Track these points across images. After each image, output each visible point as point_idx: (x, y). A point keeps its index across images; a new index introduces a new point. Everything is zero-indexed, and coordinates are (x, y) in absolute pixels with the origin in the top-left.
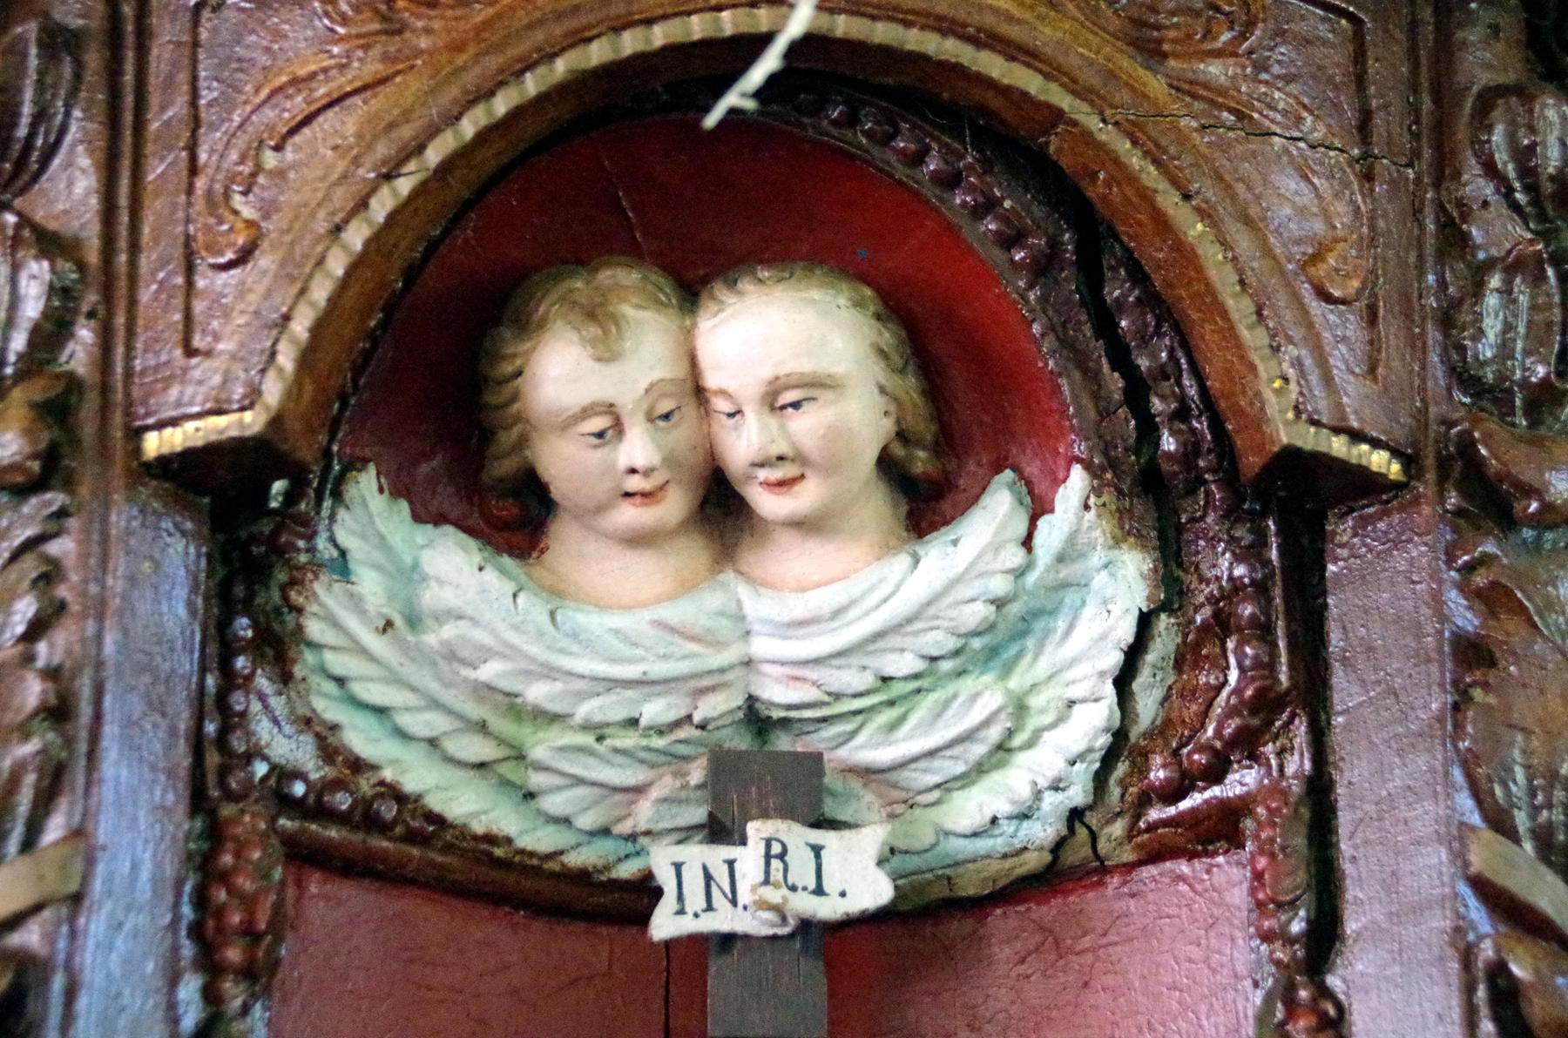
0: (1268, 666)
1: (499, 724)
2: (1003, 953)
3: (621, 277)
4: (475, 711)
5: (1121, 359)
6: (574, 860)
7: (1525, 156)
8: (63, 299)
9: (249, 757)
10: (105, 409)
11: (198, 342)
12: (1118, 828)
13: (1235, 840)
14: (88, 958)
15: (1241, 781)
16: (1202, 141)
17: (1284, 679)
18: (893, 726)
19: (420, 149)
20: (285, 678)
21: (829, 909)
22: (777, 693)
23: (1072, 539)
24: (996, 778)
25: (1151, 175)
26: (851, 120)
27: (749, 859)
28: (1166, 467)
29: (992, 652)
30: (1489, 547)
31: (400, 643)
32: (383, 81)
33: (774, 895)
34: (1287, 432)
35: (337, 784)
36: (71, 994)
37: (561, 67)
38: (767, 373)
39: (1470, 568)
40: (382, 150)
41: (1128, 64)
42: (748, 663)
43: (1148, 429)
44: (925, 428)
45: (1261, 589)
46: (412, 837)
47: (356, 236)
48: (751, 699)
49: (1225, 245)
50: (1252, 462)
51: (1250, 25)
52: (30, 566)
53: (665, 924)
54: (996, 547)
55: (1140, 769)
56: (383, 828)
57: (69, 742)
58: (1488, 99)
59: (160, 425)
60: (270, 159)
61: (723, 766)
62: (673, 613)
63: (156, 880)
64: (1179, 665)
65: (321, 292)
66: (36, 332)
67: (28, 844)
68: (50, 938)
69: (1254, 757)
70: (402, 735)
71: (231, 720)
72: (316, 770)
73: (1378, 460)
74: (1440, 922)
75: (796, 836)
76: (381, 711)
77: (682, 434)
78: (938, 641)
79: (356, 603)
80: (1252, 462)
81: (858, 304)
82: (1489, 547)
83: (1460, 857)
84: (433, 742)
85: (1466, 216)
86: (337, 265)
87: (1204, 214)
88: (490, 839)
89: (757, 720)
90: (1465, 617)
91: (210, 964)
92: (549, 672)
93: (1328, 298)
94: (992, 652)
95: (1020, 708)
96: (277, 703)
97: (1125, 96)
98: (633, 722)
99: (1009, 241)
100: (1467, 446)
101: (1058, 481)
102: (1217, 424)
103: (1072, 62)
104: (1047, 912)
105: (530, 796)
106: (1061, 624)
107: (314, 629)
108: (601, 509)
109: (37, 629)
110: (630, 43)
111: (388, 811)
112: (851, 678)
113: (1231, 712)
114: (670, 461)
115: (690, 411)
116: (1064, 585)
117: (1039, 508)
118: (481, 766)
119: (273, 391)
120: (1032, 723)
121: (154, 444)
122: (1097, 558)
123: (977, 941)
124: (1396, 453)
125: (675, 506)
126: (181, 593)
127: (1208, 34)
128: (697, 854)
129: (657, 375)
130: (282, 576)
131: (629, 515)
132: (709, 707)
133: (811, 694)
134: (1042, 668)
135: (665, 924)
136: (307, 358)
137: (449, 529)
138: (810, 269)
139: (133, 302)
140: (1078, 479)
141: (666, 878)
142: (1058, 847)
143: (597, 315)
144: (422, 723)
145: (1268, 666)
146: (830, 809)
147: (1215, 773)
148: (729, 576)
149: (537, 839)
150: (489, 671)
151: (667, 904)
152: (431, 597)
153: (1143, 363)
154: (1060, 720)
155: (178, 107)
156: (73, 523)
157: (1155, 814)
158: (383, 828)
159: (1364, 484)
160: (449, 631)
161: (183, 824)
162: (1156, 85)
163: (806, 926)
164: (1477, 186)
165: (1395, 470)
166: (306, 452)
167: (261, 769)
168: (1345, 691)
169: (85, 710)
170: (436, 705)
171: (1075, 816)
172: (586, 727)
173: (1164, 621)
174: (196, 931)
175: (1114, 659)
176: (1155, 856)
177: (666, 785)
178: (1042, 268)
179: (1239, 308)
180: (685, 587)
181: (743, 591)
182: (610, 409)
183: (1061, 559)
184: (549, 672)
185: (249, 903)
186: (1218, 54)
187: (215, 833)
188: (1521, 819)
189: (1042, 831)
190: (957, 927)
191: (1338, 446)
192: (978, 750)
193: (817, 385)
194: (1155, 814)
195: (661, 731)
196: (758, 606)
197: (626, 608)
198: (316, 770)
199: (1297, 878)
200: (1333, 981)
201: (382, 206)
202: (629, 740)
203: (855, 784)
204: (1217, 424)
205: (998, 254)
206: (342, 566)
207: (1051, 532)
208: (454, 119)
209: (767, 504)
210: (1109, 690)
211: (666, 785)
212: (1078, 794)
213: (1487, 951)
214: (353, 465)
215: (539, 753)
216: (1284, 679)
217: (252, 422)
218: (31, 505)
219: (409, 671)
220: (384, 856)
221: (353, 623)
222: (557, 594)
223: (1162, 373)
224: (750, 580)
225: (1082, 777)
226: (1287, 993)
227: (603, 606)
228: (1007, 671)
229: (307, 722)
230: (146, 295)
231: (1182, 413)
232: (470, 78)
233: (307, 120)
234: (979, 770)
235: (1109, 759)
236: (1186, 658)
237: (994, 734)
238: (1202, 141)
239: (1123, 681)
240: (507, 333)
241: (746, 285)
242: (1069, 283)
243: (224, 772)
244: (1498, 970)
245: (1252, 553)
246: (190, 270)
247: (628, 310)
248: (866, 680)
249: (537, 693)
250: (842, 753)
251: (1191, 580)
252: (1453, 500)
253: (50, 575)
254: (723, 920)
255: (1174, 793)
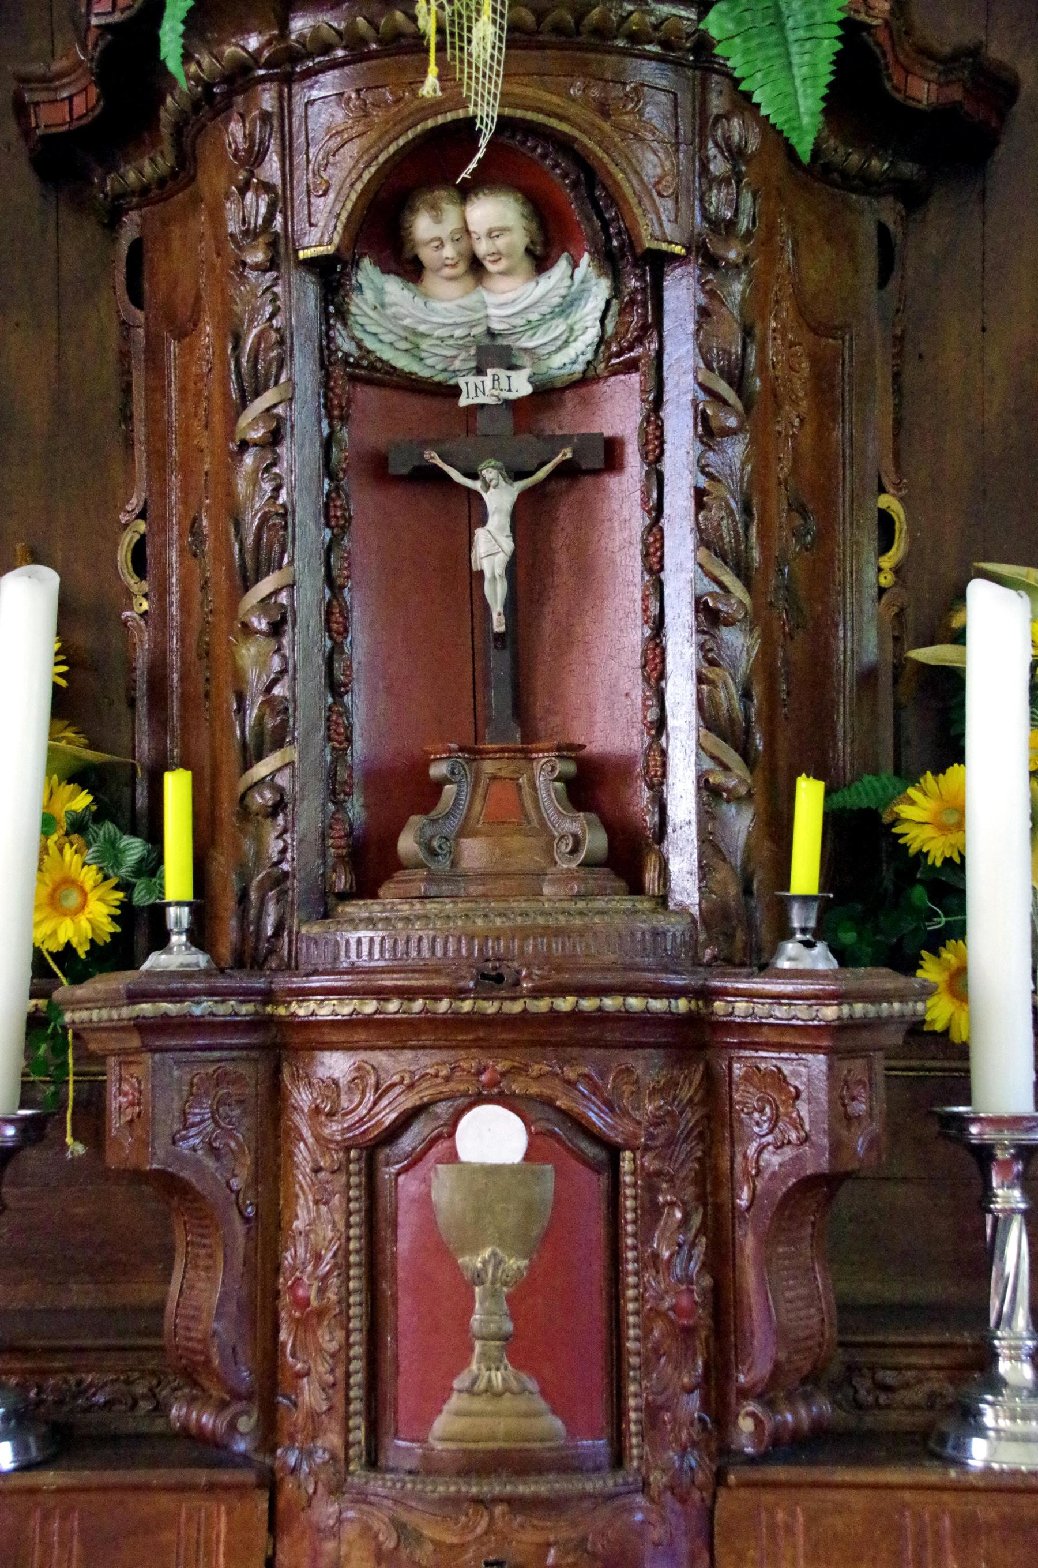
0: (645, 316)
1: (411, 338)
2: (570, 405)
3: (441, 193)
4: (403, 334)
5: (600, 216)
6: (437, 379)
7: (727, 139)
8: (272, 207)
9: (336, 351)
10: (287, 245)
11: (313, 221)
12: (603, 366)
13: (637, 369)
14: (296, 416)
15: (638, 351)
16: (622, 145)
17: (650, 320)
18: (533, 335)
19: (377, 157)
20: (345, 324)
21: (512, 396)
22: (497, 326)
23: (585, 276)
24: (564, 351)
25: (606, 159)
26: (513, 137)
27: (488, 380)
28: (615, 251)
29: (563, 311)
30: (710, 276)
31: (379, 313)
32: (364, 133)
33: (495, 392)
34: (649, 244)
35: (363, 358)
36: (292, 427)
37: (419, 128)
38: (488, 227)
39: (706, 282)
40: (366, 158)
41: (599, 121)
42: (487, 316)
43: (609, 239)
44: (539, 239)
45: (644, 290)
46: (387, 373)
47: (359, 187)
48: (489, 328)
49: (629, 181)
50: (639, 251)
51: (638, 101)
52: (269, 296)
53: (463, 402)
54: (562, 279)
55: (609, 348)
56: (378, 370)
57: (284, 352)
58: (718, 118)
59: (303, 249)
60: (331, 159)
61: (481, 350)
62: (466, 301)
63: (313, 393)
64: (619, 315)
65: (349, 206)
66: (264, 218)
67: (276, 383)
68: (285, 411)
69: (642, 343)
70: (381, 341)
71: (331, 340)
72: (356, 353)
73: (678, 250)
74: (690, 397)
75: (502, 373)
76: (375, 334)
77: (463, 245)
78: (545, 309)
79: (365, 301)
80: (639, 251)
81: (517, 200)
82: (710, 276)
83: (696, 378)
84: (391, 344)
85: (709, 161)
86: (354, 196)
87: (624, 172)
88: (411, 373)
89: (491, 334)
90: (702, 299)
91: (330, 417)
92: (425, 322)
93: (662, 196)
94: (563, 311)
95: (571, 329)
96: (344, 333)
97: (597, 132)
98: (452, 336)
99: (565, 176)
100: (704, 243)
101: (581, 257)
102: (629, 237)
103: (579, 121)
104: (583, 391)
105: (421, 359)
106: (583, 303)
107: (353, 309)
108: (439, 270)
109: (273, 316)
110: (440, 120)
111: (379, 365)
112: (519, 321)
113: (635, 330)
114: (459, 254)
115: (465, 238)
116: (583, 291)
117: (575, 265)
118: (406, 351)
119: (336, 239)
120: (576, 334)
121: (302, 255)
122: (593, 281)
123: (562, 402)
124: (683, 246)
125: (461, 268)
126: (313, 303)
127: (624, 106)
128: (472, 379)
129: (454, 227)
130: (342, 293)
131: (447, 272)
132: (475, 331)
133: (507, 326)
134: (578, 316)
135: (463, 402)
136: (346, 228)
137: (392, 276)
138: (500, 189)
139: (292, 207)
140: (586, 257)
141: (463, 386)
142: (584, 372)
143: (434, 207)
144: (388, 338)
145: (645, 316)
146: (514, 361)
147: (631, 349)
148: (480, 288)
149: (425, 373)
150: (407, 322)
151: (464, 395)
152: (388, 299)
153: (607, 216)
154: (584, 333)
155: (303, 138)
156: (280, 282)
157: (614, 361)
158: (378, 370)
159: (673, 257)
160: (394, 310)
161: (319, 374)
162: (606, 127)
163: (507, 402)
164: (712, 151)
165: (683, 252)
166: (347, 256)
167: (340, 354)
168: (668, 323)
169: (288, 341)
170: (391, 332)
171: (589, 363)
172: (438, 338)
173: (614, 301)
174: (325, 406)
175: (599, 314)
176: (615, 373)
177: (463, 355)
178: (575, 185)
179: (633, 201)
180: (467, 293)
181: (484, 293)
182: (439, 239)
183: (582, 282)
184: (425, 322)
185: (339, 397)
186: (627, 113)
187: (328, 376)
188: (715, 364)
189: (579, 367)
190: (554, 397)
191: (664, 246)
192: (559, 343)
193: (504, 230)
194: (614, 361)
195: (461, 338)
196: (490, 299)
197: (450, 300)
198: (356, 353)
199: (651, 383)
200: (661, 414)
201: (366, 176)
202: (451, 342)
203: (522, 353)
204: (629, 237)
205: (559, 180)
206: (360, 288)
207: (579, 273)
208: (387, 147)
209: (491, 267)
210: (598, 323)
211: (463, 355)
212: (589, 356)
213: (701, 407)
214: (362, 256)
215: (423, 346)
216: (650, 320)
217: (330, 249)
218: (268, 275)
219: (382, 321)
220: (378, 379)
221: (365, 308)
222: (426, 296)
223: (613, 220)
224: (489, 291)
225: (590, 351)
226: (647, 419)
227: (442, 300)
228: (567, 318)
229: (353, 338)
230: (297, 203)
231: (619, 233)
232: (392, 133)
233: (342, 146)
234: (560, 349)
235: (598, 346)
236: (621, 313)
237: (564, 337)
238: (622, 145)
239: (602, 321)
240: (407, 212)
241: (481, 195)
242: (583, 190)
243: (329, 356)
244: (704, 411)
245: (641, 278)
246: (309, 197)
247: (444, 205)
248: (524, 322)
249: (422, 328)
250: (518, 344)
251: (622, 287)
252: (700, 261)
253: (275, 297)
254: (481, 400)
255: (618, 354)
